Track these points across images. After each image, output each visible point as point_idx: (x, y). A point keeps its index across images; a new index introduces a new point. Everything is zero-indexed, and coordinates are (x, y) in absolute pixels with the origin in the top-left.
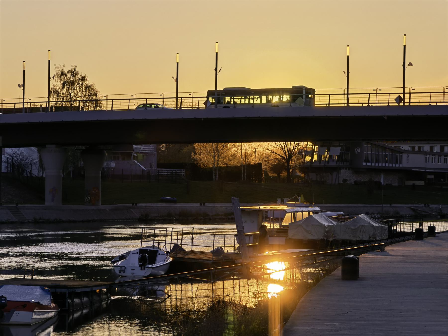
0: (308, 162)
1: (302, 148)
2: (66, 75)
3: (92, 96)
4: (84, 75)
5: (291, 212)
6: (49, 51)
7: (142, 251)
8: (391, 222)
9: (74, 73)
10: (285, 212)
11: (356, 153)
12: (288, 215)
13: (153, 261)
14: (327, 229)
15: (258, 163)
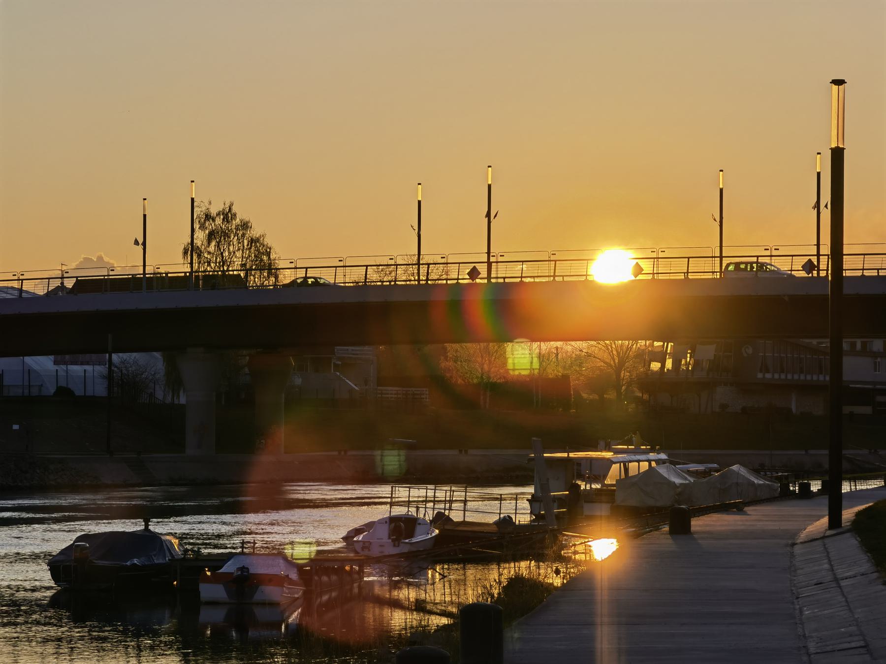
0: (654, 373)
1: (644, 348)
2: (214, 220)
3: (261, 258)
4: (247, 219)
5: (620, 462)
6: (192, 181)
7: (393, 520)
8: (787, 477)
9: (228, 215)
10: (610, 462)
11: (745, 355)
12: (615, 467)
13: (411, 535)
14: (679, 490)
15: (563, 376)
